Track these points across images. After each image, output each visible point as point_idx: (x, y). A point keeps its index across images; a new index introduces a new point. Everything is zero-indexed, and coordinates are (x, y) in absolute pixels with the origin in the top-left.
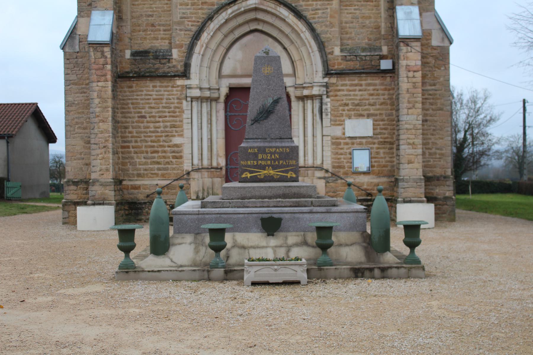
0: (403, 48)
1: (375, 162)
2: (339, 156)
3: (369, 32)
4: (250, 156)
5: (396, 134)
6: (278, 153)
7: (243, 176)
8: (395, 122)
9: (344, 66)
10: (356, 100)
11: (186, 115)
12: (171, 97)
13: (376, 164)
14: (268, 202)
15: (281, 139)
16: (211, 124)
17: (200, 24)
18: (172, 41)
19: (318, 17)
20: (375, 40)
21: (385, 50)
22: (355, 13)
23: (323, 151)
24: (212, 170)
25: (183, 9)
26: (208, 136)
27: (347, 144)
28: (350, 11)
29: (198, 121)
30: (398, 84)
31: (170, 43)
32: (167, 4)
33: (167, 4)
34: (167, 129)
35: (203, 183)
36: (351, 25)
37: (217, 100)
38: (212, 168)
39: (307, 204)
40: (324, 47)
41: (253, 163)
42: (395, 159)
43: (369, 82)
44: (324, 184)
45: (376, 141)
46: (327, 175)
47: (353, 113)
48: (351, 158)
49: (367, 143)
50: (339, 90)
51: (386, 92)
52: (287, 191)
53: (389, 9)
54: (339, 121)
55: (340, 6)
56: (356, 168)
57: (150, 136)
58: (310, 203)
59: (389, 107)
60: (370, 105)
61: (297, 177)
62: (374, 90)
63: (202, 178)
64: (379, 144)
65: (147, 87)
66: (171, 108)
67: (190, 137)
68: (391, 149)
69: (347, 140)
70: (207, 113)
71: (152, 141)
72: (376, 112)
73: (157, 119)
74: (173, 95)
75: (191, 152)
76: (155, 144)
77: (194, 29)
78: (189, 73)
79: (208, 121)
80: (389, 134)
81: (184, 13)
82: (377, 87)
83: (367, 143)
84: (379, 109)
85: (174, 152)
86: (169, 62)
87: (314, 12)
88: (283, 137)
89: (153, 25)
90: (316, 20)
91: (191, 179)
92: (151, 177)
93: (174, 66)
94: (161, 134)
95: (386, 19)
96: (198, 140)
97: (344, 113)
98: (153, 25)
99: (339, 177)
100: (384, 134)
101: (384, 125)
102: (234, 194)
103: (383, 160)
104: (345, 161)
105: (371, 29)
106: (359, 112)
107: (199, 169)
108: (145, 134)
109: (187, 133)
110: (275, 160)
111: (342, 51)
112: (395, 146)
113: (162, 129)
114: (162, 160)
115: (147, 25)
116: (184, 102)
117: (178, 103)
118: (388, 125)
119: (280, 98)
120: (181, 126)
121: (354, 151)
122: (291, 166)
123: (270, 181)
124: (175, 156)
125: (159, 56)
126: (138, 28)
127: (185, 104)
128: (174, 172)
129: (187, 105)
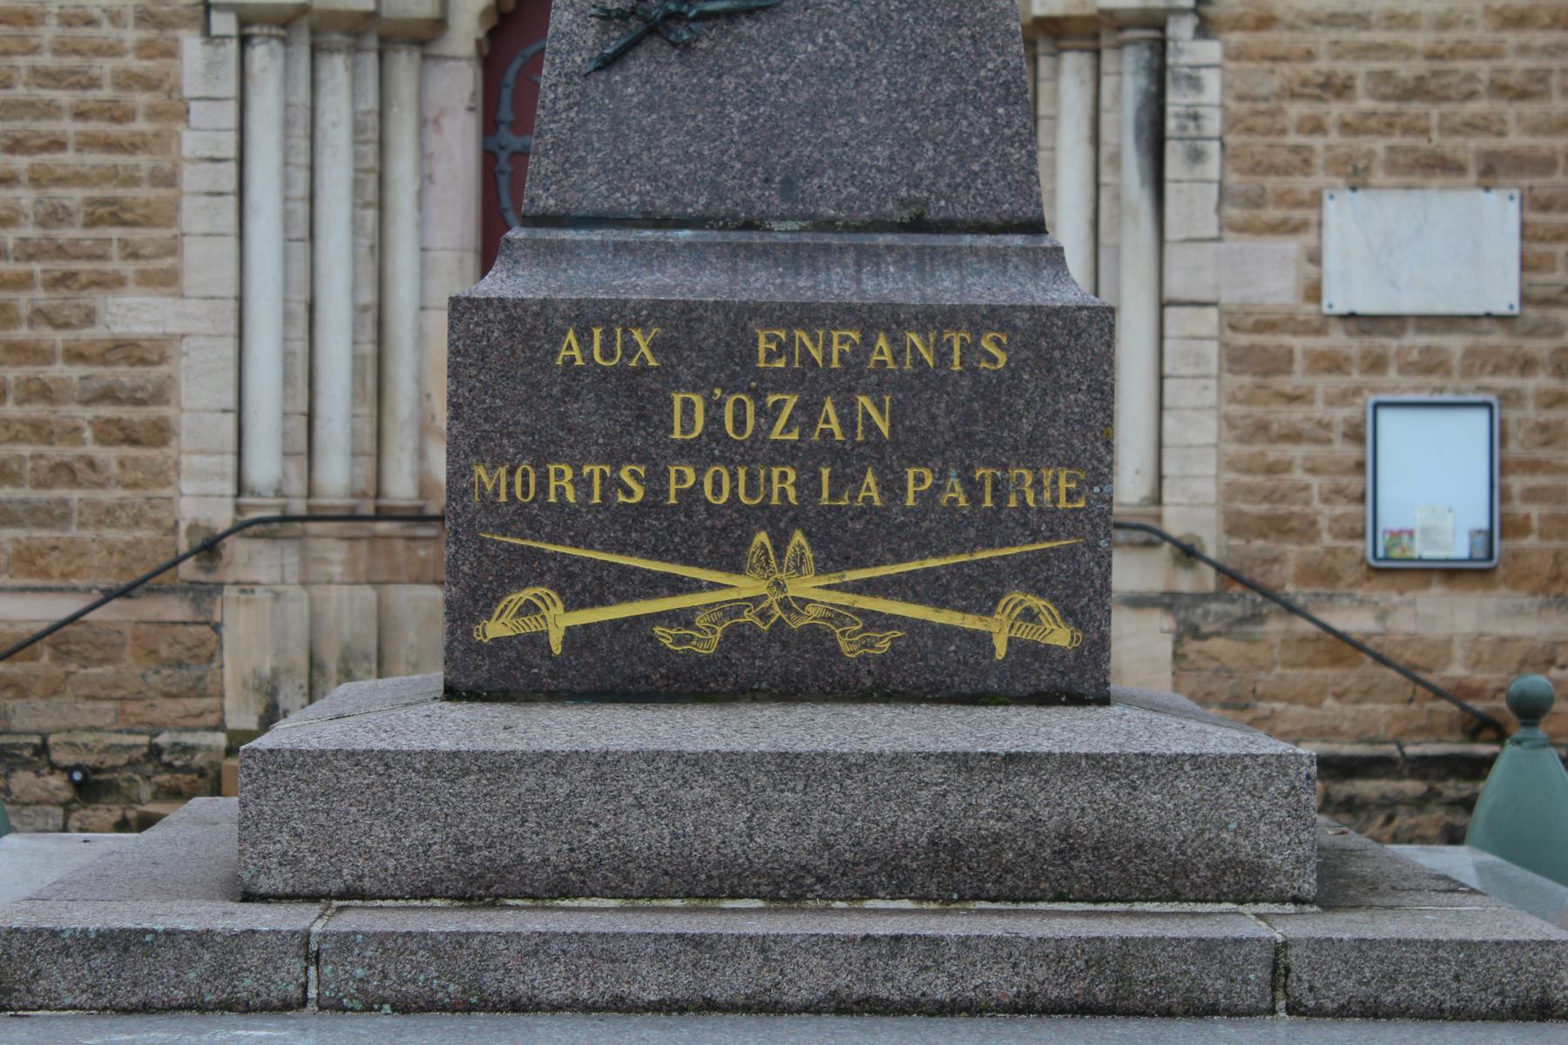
1: (1531, 495)
2: (1275, 453)
4: (580, 411)
6: (880, 383)
7: (496, 628)
10: (1408, 52)
11: (204, 135)
13: (1535, 511)
14: (763, 945)
15: (918, 225)
16: (381, 206)
23: (1161, 408)
24: (383, 527)
26: (355, 289)
27: (1333, 364)
29: (287, 183)
34: (65, 234)
35: (314, 619)
37: (425, 37)
38: (381, 515)
39: (1216, 985)
41: (612, 484)
44: (1166, 647)
45: (1540, 347)
46: (1185, 582)
47: (1379, 145)
48: (1360, 466)
49: (1476, 361)
52: (981, 812)
54: (1284, 199)
56: (1396, 535)
58: (1259, 974)
60: (1499, 89)
61: (1097, 648)
63: (304, 583)
66: (94, 83)
67: (232, 291)
69: (1338, 340)
70: (357, 129)
72: (1544, 143)
75: (229, 400)
79: (357, 185)
83: (1476, 361)
85: (108, 395)
88: (938, 209)
91: (231, 592)
94: (22, 267)
96: (287, 318)
97: (1317, 142)
99: (1270, 595)
102: (382, 831)
104: (1315, 482)
106: (1421, 142)
107: (286, 519)
109: (204, 261)
110: (847, 461)
113: (30, 231)
114: (26, 450)
116: (191, 45)
117: (144, 50)
120: (167, 215)
121: (1385, 416)
122: (1028, 524)
123: (789, 692)
124: (117, 422)
127: (197, 62)
128: (110, 534)
129: (211, 66)
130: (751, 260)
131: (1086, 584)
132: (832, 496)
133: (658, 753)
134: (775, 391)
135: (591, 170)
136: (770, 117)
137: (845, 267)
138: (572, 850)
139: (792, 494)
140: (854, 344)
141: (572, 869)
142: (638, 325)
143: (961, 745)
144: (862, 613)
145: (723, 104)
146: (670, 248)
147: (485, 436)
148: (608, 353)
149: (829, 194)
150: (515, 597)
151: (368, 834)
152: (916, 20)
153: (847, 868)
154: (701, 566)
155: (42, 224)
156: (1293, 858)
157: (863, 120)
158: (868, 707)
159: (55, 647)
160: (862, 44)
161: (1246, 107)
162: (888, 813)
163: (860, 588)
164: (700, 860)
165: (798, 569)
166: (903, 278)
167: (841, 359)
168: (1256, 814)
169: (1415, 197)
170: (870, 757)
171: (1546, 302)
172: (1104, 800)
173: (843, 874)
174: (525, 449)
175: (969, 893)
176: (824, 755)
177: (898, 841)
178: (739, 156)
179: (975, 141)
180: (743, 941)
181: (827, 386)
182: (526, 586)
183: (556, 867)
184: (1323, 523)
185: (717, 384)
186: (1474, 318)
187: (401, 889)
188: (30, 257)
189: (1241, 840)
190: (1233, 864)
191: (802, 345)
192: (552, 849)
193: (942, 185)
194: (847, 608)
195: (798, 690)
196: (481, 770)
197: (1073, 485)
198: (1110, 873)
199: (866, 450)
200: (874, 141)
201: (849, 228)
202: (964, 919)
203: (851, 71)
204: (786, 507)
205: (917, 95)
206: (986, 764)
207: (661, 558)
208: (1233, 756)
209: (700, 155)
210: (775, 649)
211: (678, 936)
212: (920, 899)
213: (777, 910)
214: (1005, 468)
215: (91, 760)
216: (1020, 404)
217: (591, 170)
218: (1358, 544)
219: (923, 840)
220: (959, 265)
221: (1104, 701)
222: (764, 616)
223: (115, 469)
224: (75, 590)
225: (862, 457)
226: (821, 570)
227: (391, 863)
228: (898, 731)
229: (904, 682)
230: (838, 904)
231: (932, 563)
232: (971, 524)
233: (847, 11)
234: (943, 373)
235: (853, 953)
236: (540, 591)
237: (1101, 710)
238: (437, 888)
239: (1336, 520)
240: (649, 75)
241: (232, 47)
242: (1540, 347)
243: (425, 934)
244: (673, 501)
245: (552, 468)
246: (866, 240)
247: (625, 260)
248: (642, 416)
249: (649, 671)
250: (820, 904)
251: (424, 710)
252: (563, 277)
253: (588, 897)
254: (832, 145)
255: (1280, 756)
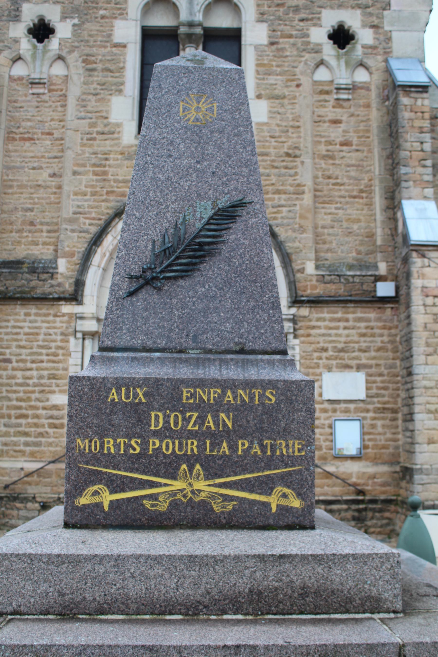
0: (417, 262)
1: (370, 440)
3: (357, 242)
4: (116, 419)
5: (403, 395)
7: (84, 500)
8: (399, 378)
9: (319, 290)
10: (340, 342)
12: (51, 331)
15: (242, 351)
17: (102, 222)
18: (59, 247)
19: (282, 218)
20: (367, 254)
21: (383, 268)
22: (337, 214)
25: (78, 200)
28: (329, 211)
30: (409, 317)
31: (56, 251)
32: (55, 193)
33: (55, 193)
34: (43, 381)
36: (331, 231)
40: (290, 261)
41: (128, 446)
42: (400, 436)
43: (359, 315)
45: (370, 407)
47: (334, 362)
50: (314, 327)
51: (386, 332)
52: (270, 579)
53: (388, 208)
54: (314, 374)
55: (315, 202)
56: (340, 449)
57: (15, 392)
59: (390, 354)
60: (360, 350)
62: (367, 328)
64: (375, 412)
65: (16, 314)
66: (50, 348)
68: (394, 419)
71: (18, 400)
73: (29, 365)
74: (55, 328)
76: (23, 404)
77: (94, 230)
78: (82, 295)
80: (391, 396)
81: (79, 206)
82: (372, 324)
83: (357, 410)
84: (374, 358)
85: (51, 417)
86: (52, 277)
87: (275, 210)
88: (249, 346)
89: (32, 224)
90: (279, 221)
92: (13, 456)
93: (59, 285)
95: (383, 222)
97: (320, 362)
98: (32, 224)
100: (383, 396)
101: (382, 382)
102: (29, 587)
103: (382, 437)
105: (360, 238)
108: (9, 388)
110: (216, 437)
111: (317, 267)
112: (400, 415)
113: (35, 381)
114: (33, 429)
115: (23, 223)
116: (72, 340)
117: (62, 341)
118: (389, 382)
119: (241, 204)
122: (284, 461)
123: (194, 525)
125: (37, 268)
126: (9, 227)
128: (52, 449)
129: (76, 345)
130: (181, 363)
131: (305, 484)
132: (211, 451)
133: (141, 555)
134: (189, 411)
135: (124, 331)
136: (189, 313)
137: (215, 366)
138: (105, 595)
139: (195, 450)
140: (219, 394)
141: (105, 603)
142: (139, 386)
143: (261, 551)
144: (222, 495)
145: (172, 309)
146: (152, 359)
147: (81, 428)
148: (127, 397)
149: (210, 340)
150: (91, 489)
151: (23, 588)
152: (241, 280)
153: (216, 602)
154: (161, 477)
155: (38, 379)
156: (392, 595)
157: (222, 314)
158: (224, 531)
159: (38, 474)
160: (222, 288)
161: (304, 354)
162: (233, 579)
163: (220, 486)
164: (157, 599)
165: (198, 478)
166: (236, 370)
167: (214, 400)
168: (378, 577)
169: (343, 373)
170: (226, 557)
171: (372, 397)
172: (318, 573)
173: (215, 604)
174: (96, 433)
175: (265, 612)
176: (207, 556)
177: (237, 591)
178: (177, 327)
179: (262, 322)
180: (171, 648)
181: (209, 409)
182: (95, 484)
183: (99, 602)
184: (324, 447)
185: (168, 408)
186: (356, 400)
187: (36, 611)
188: (35, 386)
189: (372, 588)
190: (369, 598)
191: (200, 394)
192: (97, 595)
193: (250, 337)
194: (216, 493)
195: (198, 524)
196: (69, 562)
197: (300, 446)
198: (321, 603)
199: (223, 434)
200: (226, 322)
201: (217, 352)
202: (265, 628)
203: (218, 298)
204: (193, 455)
205: (241, 306)
206: (271, 559)
207: (146, 474)
208: (369, 554)
209: (164, 326)
210: (189, 509)
211: (143, 646)
212: (245, 614)
213: (188, 621)
214: (275, 440)
215: (45, 500)
216: (280, 416)
217: (124, 331)
218: (331, 451)
219: (247, 590)
220: (257, 366)
221: (313, 528)
222: (185, 496)
223: (52, 434)
224: (42, 461)
225: (222, 436)
226: (207, 479)
227: (32, 600)
228: (236, 543)
229: (238, 522)
230: (213, 617)
231: (248, 476)
232: (262, 461)
233: (216, 277)
234: (252, 405)
235: (219, 653)
236: (101, 486)
237: (312, 531)
238: (51, 610)
239: (326, 446)
240: (146, 298)
241: (81, 340)
242: (370, 407)
243: (32, 646)
244: (151, 452)
245: (106, 440)
246: (223, 356)
247: (135, 364)
248: (140, 420)
249: (141, 517)
250: (205, 617)
251: (54, 532)
252: (112, 369)
253: (111, 614)
254: (211, 323)
255: (386, 554)
